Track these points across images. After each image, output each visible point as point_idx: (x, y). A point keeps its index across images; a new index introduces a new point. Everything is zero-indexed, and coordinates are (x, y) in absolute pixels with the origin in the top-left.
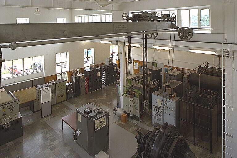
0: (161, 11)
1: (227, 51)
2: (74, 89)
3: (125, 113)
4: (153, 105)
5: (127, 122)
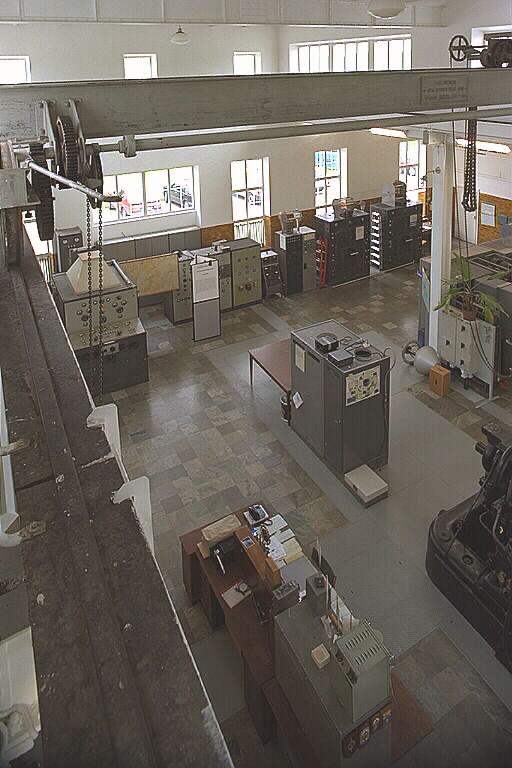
2: (285, 277)
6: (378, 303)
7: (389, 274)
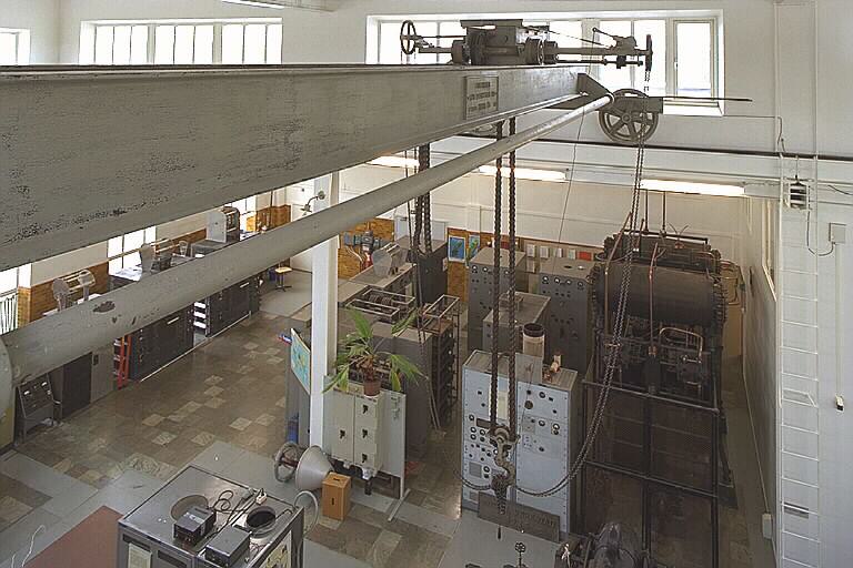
0: (633, 20)
1: (798, 184)
2: (60, 389)
3: (337, 466)
5: (350, 514)
6: (217, 390)
7: (218, 340)
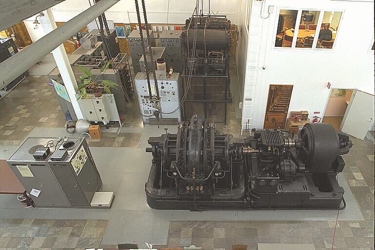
4: (139, 96)
